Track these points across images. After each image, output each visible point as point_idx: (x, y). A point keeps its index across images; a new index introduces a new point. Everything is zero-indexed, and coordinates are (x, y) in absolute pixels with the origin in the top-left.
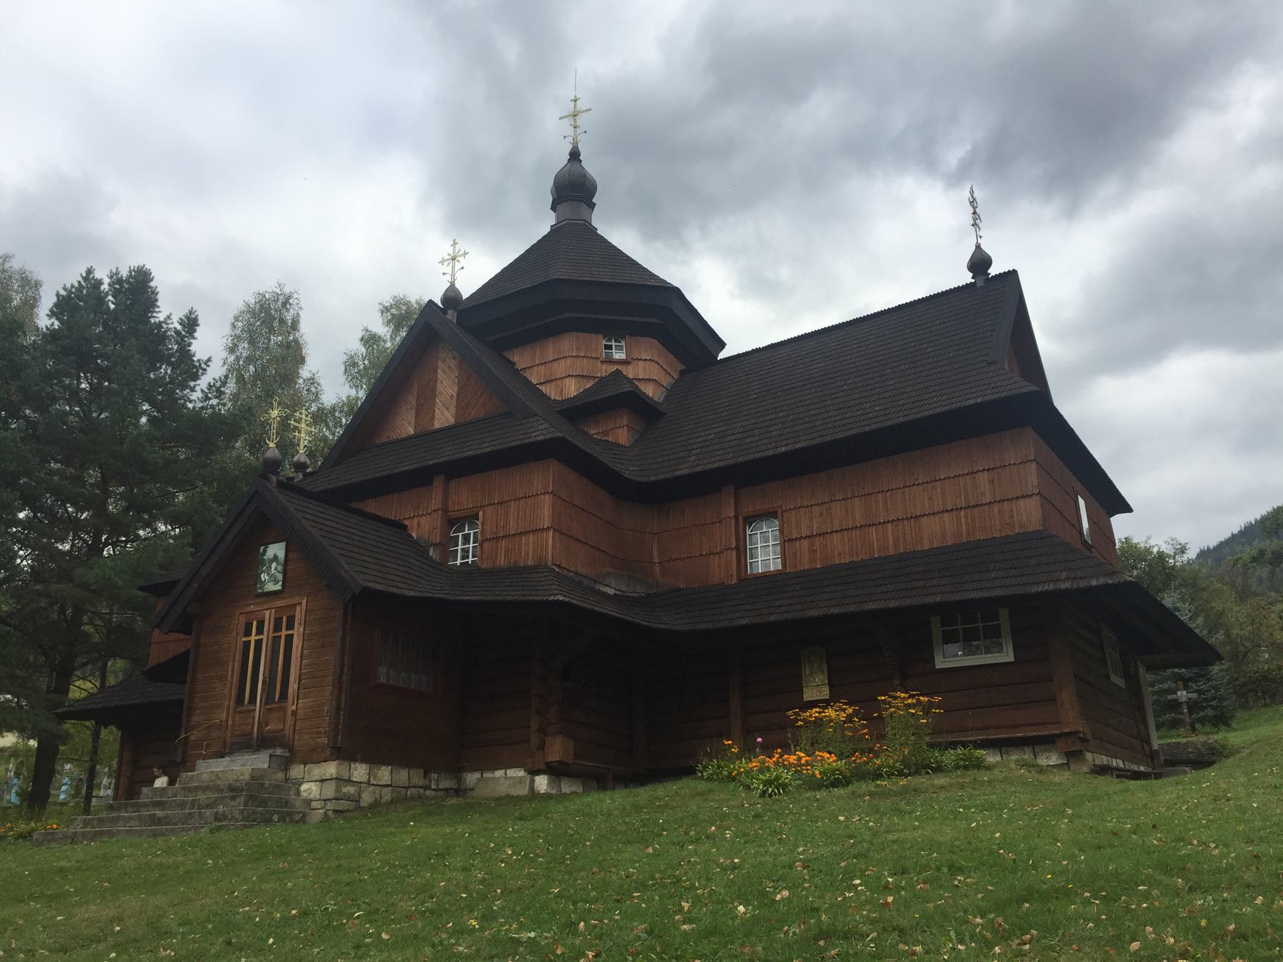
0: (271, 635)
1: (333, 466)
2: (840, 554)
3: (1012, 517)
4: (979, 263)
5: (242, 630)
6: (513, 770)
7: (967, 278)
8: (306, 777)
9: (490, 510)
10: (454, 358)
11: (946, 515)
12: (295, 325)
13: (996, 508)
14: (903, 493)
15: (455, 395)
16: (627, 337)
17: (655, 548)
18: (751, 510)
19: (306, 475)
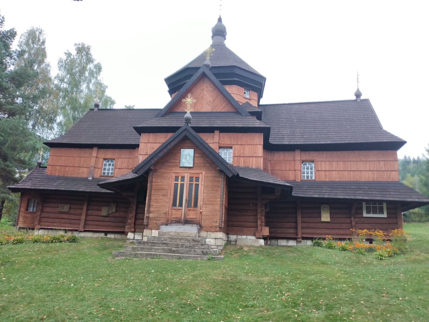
0: (188, 183)
1: (162, 117)
2: (335, 178)
3: (390, 176)
4: (358, 95)
5: (174, 178)
6: (250, 236)
7: (354, 98)
8: (208, 236)
9: (237, 146)
10: (211, 87)
11: (370, 172)
12: (43, 43)
13: (385, 172)
14: (357, 163)
15: (212, 101)
16: (250, 91)
17: (269, 165)
18: (304, 159)
19: (99, 110)
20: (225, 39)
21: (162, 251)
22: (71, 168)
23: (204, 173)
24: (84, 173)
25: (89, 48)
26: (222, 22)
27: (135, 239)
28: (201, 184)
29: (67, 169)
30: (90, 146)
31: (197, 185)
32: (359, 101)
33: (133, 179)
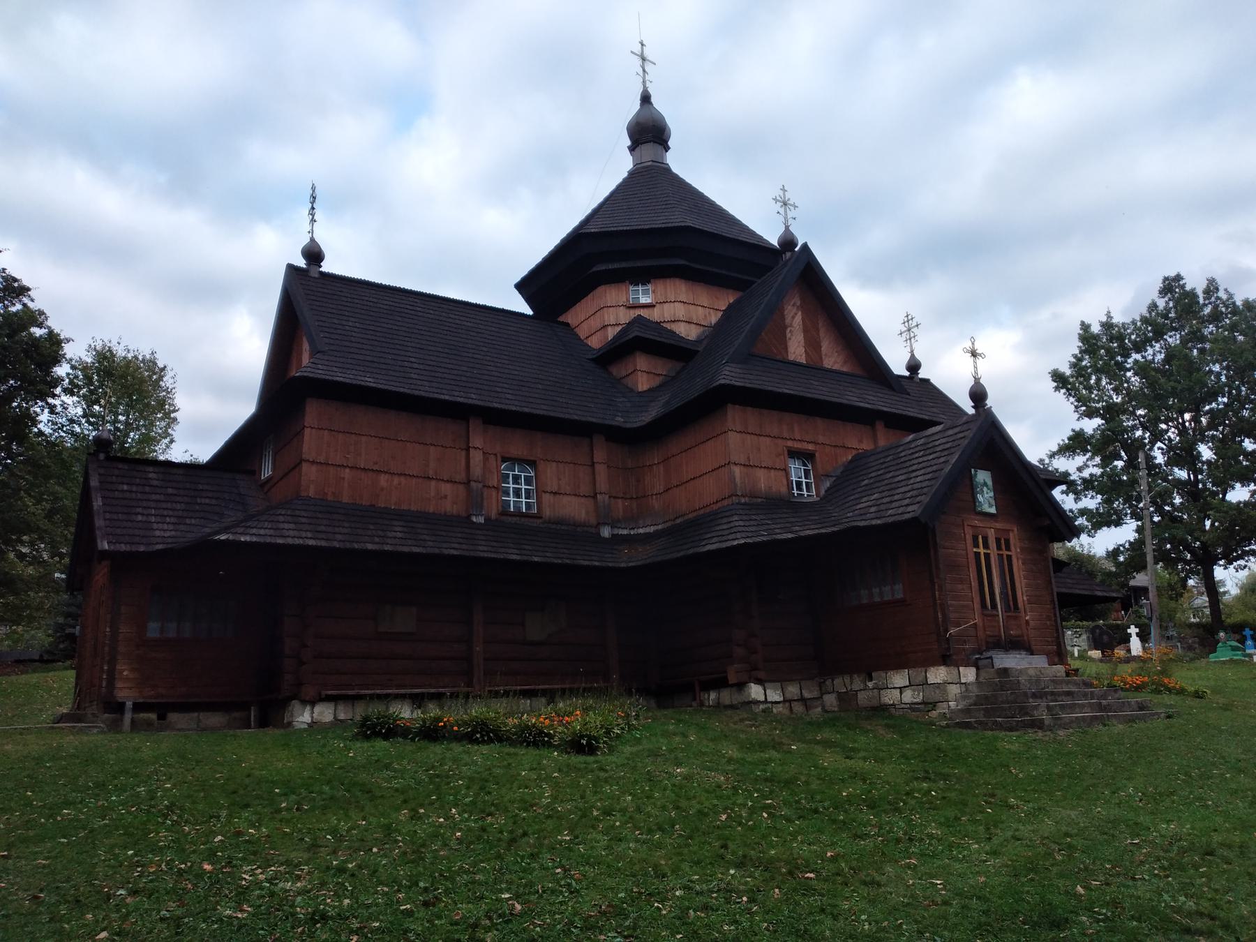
20: (667, 148)
21: (1089, 710)
22: (396, 480)
23: (1016, 529)
24: (446, 497)
25: (1166, 279)
26: (651, 103)
27: (898, 690)
28: (1015, 552)
29: (383, 480)
30: (458, 413)
31: (1009, 557)
32: (317, 276)
33: (92, 506)
